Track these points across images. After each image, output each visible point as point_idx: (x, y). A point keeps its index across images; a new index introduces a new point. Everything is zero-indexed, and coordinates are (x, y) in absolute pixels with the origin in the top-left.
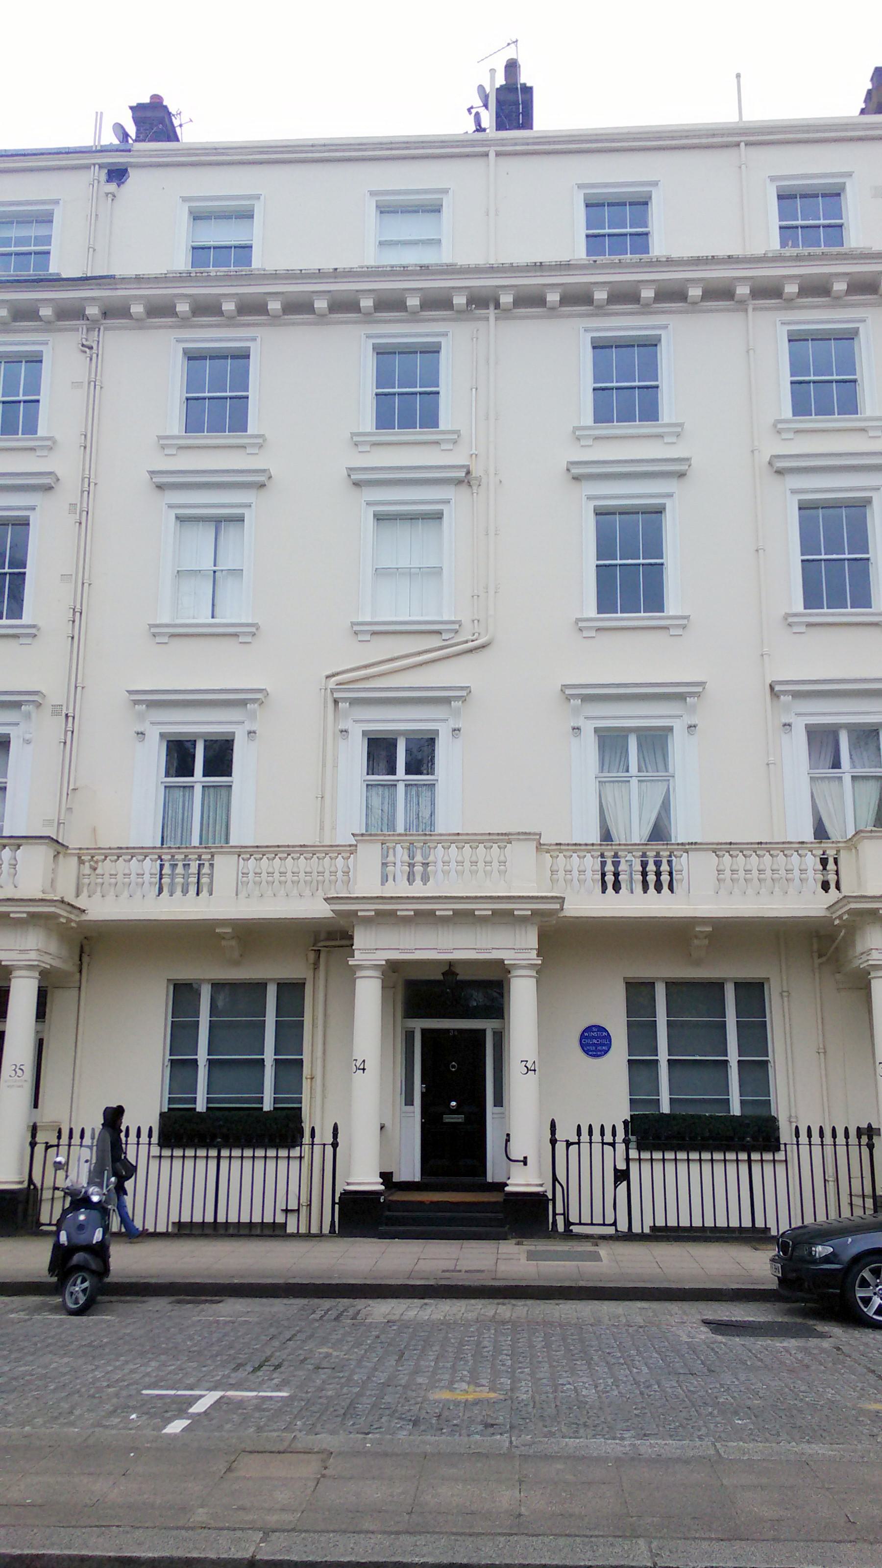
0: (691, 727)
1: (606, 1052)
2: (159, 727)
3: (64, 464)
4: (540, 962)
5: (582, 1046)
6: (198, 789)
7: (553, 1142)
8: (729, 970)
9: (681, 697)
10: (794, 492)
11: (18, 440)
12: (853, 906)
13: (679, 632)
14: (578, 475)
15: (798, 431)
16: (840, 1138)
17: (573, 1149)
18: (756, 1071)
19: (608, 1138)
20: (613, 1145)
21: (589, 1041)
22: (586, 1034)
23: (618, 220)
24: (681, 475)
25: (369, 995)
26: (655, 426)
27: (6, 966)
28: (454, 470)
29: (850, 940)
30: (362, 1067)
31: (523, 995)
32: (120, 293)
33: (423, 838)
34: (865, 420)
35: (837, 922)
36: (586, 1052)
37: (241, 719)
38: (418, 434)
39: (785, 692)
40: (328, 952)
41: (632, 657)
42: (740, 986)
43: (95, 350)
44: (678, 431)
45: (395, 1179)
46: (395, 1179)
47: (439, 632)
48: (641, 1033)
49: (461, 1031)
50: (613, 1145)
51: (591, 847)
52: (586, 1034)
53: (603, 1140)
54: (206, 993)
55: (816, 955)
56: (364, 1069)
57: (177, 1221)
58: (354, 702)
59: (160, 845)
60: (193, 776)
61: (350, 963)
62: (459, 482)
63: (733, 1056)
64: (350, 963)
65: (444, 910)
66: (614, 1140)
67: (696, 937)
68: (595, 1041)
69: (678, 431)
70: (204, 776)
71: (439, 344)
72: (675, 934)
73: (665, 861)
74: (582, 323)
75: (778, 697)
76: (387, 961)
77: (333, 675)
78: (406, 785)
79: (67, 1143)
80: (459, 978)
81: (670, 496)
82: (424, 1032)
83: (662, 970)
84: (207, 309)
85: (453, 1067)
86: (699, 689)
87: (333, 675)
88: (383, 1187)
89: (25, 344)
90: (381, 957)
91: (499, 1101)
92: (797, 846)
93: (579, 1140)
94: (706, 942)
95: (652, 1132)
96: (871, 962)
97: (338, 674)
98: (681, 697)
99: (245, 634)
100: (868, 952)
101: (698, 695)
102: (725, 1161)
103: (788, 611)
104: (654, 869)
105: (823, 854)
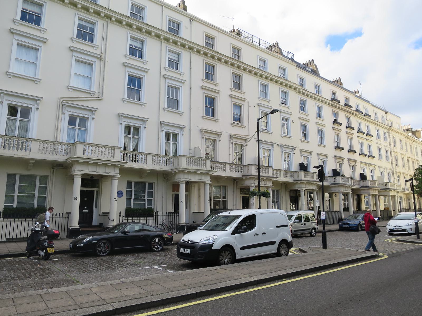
0: (37, 109)
1: (122, 196)
3: (185, 77)
6: (18, 121)
7: (120, 216)
8: (147, 180)
11: (26, 23)
12: (72, 159)
13: (38, 83)
14: (44, 41)
16: (58, 216)
18: (150, 201)
26: (39, 27)
27: (178, 182)
28: (45, 39)
30: (76, 199)
34: (144, 60)
35: (68, 163)
38: (33, 25)
40: (56, 169)
42: (41, 177)
44: (45, 30)
47: (90, 93)
48: (129, 193)
49: (88, 191)
54: (38, 179)
55: (164, 178)
56: (77, 199)
57: (23, 237)
59: (4, 135)
60: (17, 117)
63: (37, 195)
65: (91, 162)
70: (20, 117)
71: (43, 5)
72: (24, 162)
73: (134, 155)
74: (129, 31)
76: (84, 174)
77: (62, 98)
78: (19, 120)
79: (62, 217)
80: (94, 178)
83: (134, 179)
85: (86, 199)
88: (79, 227)
89: (263, 82)
94: (33, 165)
95: (130, 213)
96: (75, 173)
100: (75, 171)
102: (14, 221)
104: (135, 157)
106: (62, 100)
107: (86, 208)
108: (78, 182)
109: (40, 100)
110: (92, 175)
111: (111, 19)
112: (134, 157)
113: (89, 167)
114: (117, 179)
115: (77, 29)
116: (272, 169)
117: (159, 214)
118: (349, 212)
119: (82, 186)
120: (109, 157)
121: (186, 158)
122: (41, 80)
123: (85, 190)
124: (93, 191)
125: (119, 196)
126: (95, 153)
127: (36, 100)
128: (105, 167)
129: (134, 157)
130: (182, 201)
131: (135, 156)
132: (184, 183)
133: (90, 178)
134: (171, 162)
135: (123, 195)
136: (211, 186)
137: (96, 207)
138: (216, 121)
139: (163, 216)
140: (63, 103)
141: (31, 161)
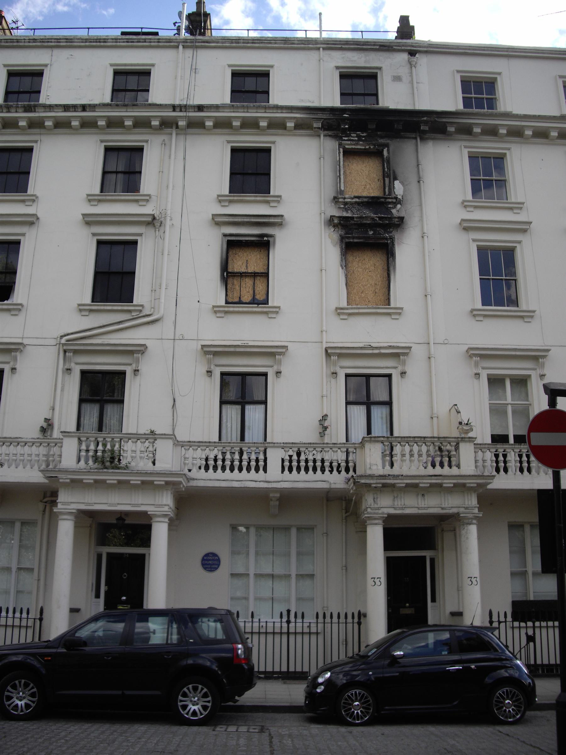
1: (216, 569)
4: (481, 515)
5: (203, 565)
9: (273, 355)
10: (474, 240)
14: (523, 228)
15: (476, 207)
21: (206, 562)
22: (205, 558)
23: (250, 85)
24: (525, 231)
25: (66, 530)
29: (358, 503)
31: (160, 533)
32: (36, 115)
35: (351, 492)
36: (205, 569)
39: (334, 354)
49: (131, 555)
51: (209, 444)
52: (205, 558)
55: (344, 511)
58: (76, 352)
61: (55, 510)
62: (148, 224)
67: (271, 500)
68: (210, 562)
69: (34, 199)
75: (330, 357)
77: (65, 336)
80: (126, 522)
82: (109, 554)
84: (114, 124)
85: (125, 576)
86: (283, 350)
87: (65, 336)
90: (74, 507)
91: (434, 600)
92: (332, 445)
94: (277, 503)
97: (68, 335)
99: (14, 309)
101: (280, 354)
103: (473, 308)
105: (496, 451)
106: (63, 341)
107: (124, 598)
108: (375, 536)
109: (280, 354)
110: (121, 512)
111: (177, 127)
112: (501, 458)
113: (469, 496)
114: (474, 521)
115: (471, 179)
116: (475, 444)
119: (387, 547)
120: (413, 468)
121: (76, 439)
123: (122, 554)
124: (425, 557)
125: (209, 566)
126: (411, 461)
127: (274, 353)
128: (463, 492)
129: (501, 458)
131: (505, 456)
133: (115, 522)
134: (513, 462)
135: (219, 565)
136: (481, 523)
137: (434, 600)
138: (527, 316)
140: (329, 351)
141: (271, 495)
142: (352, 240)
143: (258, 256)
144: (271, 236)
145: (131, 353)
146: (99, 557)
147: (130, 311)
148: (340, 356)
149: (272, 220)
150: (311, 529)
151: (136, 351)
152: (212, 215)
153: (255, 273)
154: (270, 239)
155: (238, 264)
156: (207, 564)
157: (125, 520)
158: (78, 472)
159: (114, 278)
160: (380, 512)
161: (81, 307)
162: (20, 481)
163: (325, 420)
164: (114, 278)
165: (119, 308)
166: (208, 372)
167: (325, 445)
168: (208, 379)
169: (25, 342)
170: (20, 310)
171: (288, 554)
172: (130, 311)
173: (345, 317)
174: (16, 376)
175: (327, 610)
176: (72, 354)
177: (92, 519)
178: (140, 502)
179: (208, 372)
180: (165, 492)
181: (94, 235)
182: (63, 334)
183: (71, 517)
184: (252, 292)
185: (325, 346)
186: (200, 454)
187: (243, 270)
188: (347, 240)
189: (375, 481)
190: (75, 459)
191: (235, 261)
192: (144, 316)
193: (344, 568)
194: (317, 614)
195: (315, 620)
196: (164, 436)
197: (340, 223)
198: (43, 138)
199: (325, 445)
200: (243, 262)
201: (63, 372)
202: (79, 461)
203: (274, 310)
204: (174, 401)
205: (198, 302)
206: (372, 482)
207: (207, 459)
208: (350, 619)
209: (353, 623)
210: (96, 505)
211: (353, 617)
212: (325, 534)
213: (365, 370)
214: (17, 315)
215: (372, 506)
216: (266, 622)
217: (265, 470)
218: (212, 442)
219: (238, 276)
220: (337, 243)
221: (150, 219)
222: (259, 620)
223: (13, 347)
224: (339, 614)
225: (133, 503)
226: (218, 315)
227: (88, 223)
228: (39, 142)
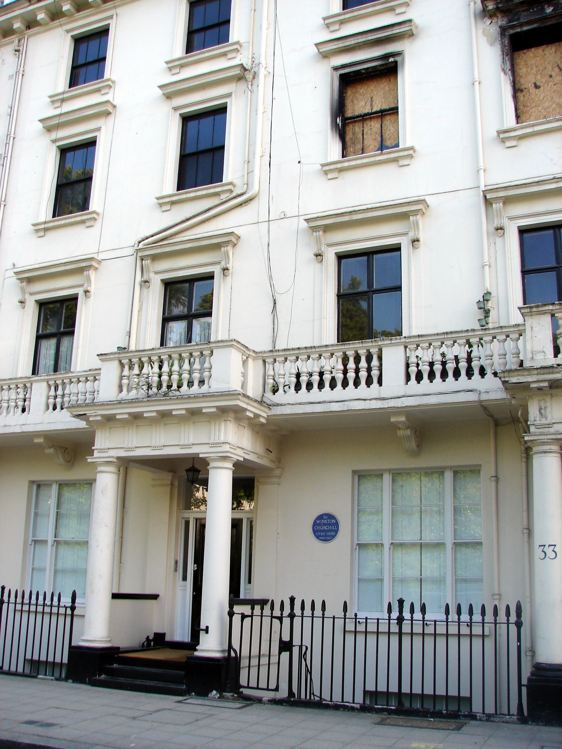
1: (333, 537)
2: (336, 248)
5: (315, 532)
9: (404, 216)
17: (247, 621)
19: (277, 613)
20: (280, 619)
33: (466, 334)
36: (318, 537)
37: (81, 283)
41: (372, 186)
43: (21, 52)
45: (168, 638)
46: (168, 638)
50: (280, 619)
53: (272, 614)
61: (89, 460)
62: (240, 78)
64: (89, 460)
66: (282, 614)
68: (325, 528)
75: (491, 204)
81: (99, 129)
93: (252, 613)
98: (404, 216)
117: (297, 610)
118: (112, 590)
122: (412, 148)
125: (323, 534)
127: (404, 213)
130: (549, 550)
132: (230, 465)
135: (337, 531)
139: (328, 623)
142: (519, 30)
143: (387, 88)
144: (399, 54)
145: (217, 247)
146: (187, 523)
147: (217, 194)
148: (507, 201)
149: (396, 30)
150: (475, 470)
151: (223, 243)
152: (316, 45)
153: (382, 111)
154: (398, 59)
155: (360, 105)
156: (321, 531)
157: (199, 471)
158: (108, 404)
159: (200, 158)
160: (552, 430)
161: (161, 201)
162: (534, 483)
163: (487, 300)
164: (200, 158)
165: (204, 192)
166: (317, 255)
167: (470, 334)
168: (318, 266)
169: (100, 257)
170: (95, 219)
171: (441, 513)
172: (217, 194)
173: (513, 143)
174: (91, 300)
175: (500, 599)
176: (149, 261)
177: (171, 474)
178: (191, 441)
179: (317, 255)
180: (223, 424)
181: (175, 109)
182: (140, 239)
183: (112, 469)
184: (379, 139)
185: (483, 188)
186: (291, 368)
187: (367, 110)
188: (512, 32)
189: (534, 378)
190: (116, 389)
191: (355, 102)
192: (235, 198)
193: (525, 531)
194: (447, 606)
195: (444, 617)
196: (221, 344)
197: (497, 9)
198: (119, 10)
199: (470, 334)
200: (363, 101)
201: (141, 287)
202: (121, 391)
203: (406, 153)
204: (275, 303)
205: (299, 162)
206: (529, 379)
207: (298, 376)
208: (502, 617)
209: (508, 624)
210: (137, 450)
211: (508, 614)
212: (494, 479)
213: (554, 216)
214: (92, 226)
215: (538, 422)
216: (366, 619)
217: (380, 382)
218: (302, 348)
219: (360, 121)
220: (496, 39)
221: (237, 71)
222: (356, 615)
223: (84, 264)
224: (483, 607)
225: (182, 443)
226: (330, 176)
227: (169, 97)
228: (115, 17)
